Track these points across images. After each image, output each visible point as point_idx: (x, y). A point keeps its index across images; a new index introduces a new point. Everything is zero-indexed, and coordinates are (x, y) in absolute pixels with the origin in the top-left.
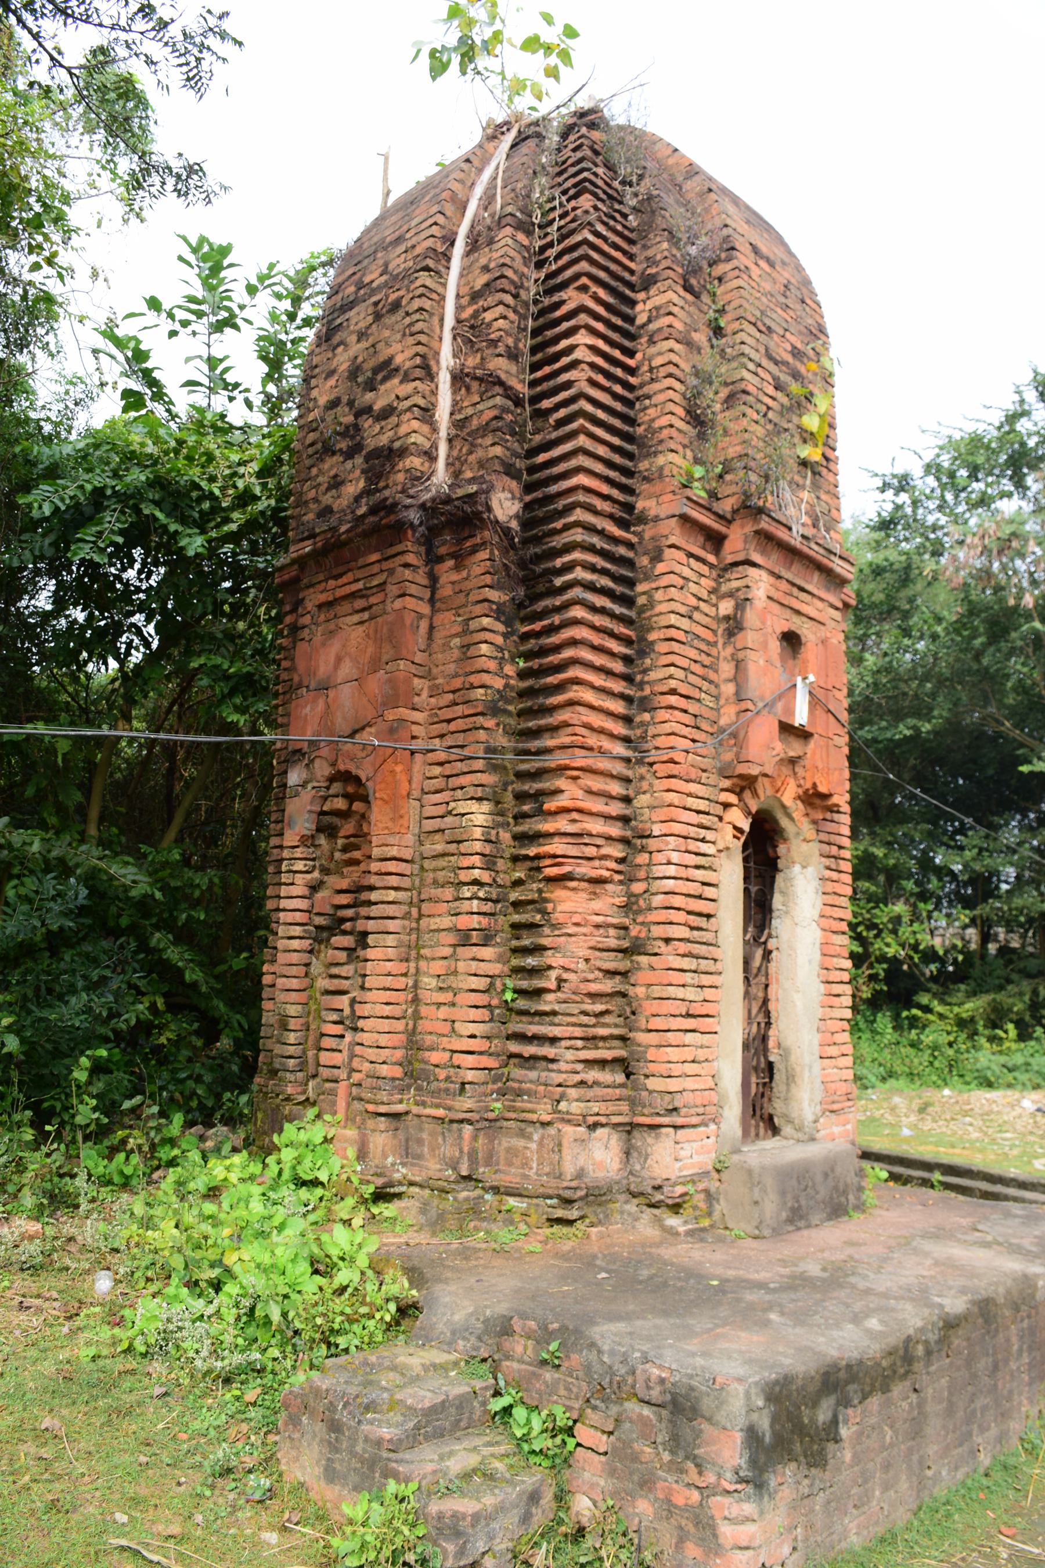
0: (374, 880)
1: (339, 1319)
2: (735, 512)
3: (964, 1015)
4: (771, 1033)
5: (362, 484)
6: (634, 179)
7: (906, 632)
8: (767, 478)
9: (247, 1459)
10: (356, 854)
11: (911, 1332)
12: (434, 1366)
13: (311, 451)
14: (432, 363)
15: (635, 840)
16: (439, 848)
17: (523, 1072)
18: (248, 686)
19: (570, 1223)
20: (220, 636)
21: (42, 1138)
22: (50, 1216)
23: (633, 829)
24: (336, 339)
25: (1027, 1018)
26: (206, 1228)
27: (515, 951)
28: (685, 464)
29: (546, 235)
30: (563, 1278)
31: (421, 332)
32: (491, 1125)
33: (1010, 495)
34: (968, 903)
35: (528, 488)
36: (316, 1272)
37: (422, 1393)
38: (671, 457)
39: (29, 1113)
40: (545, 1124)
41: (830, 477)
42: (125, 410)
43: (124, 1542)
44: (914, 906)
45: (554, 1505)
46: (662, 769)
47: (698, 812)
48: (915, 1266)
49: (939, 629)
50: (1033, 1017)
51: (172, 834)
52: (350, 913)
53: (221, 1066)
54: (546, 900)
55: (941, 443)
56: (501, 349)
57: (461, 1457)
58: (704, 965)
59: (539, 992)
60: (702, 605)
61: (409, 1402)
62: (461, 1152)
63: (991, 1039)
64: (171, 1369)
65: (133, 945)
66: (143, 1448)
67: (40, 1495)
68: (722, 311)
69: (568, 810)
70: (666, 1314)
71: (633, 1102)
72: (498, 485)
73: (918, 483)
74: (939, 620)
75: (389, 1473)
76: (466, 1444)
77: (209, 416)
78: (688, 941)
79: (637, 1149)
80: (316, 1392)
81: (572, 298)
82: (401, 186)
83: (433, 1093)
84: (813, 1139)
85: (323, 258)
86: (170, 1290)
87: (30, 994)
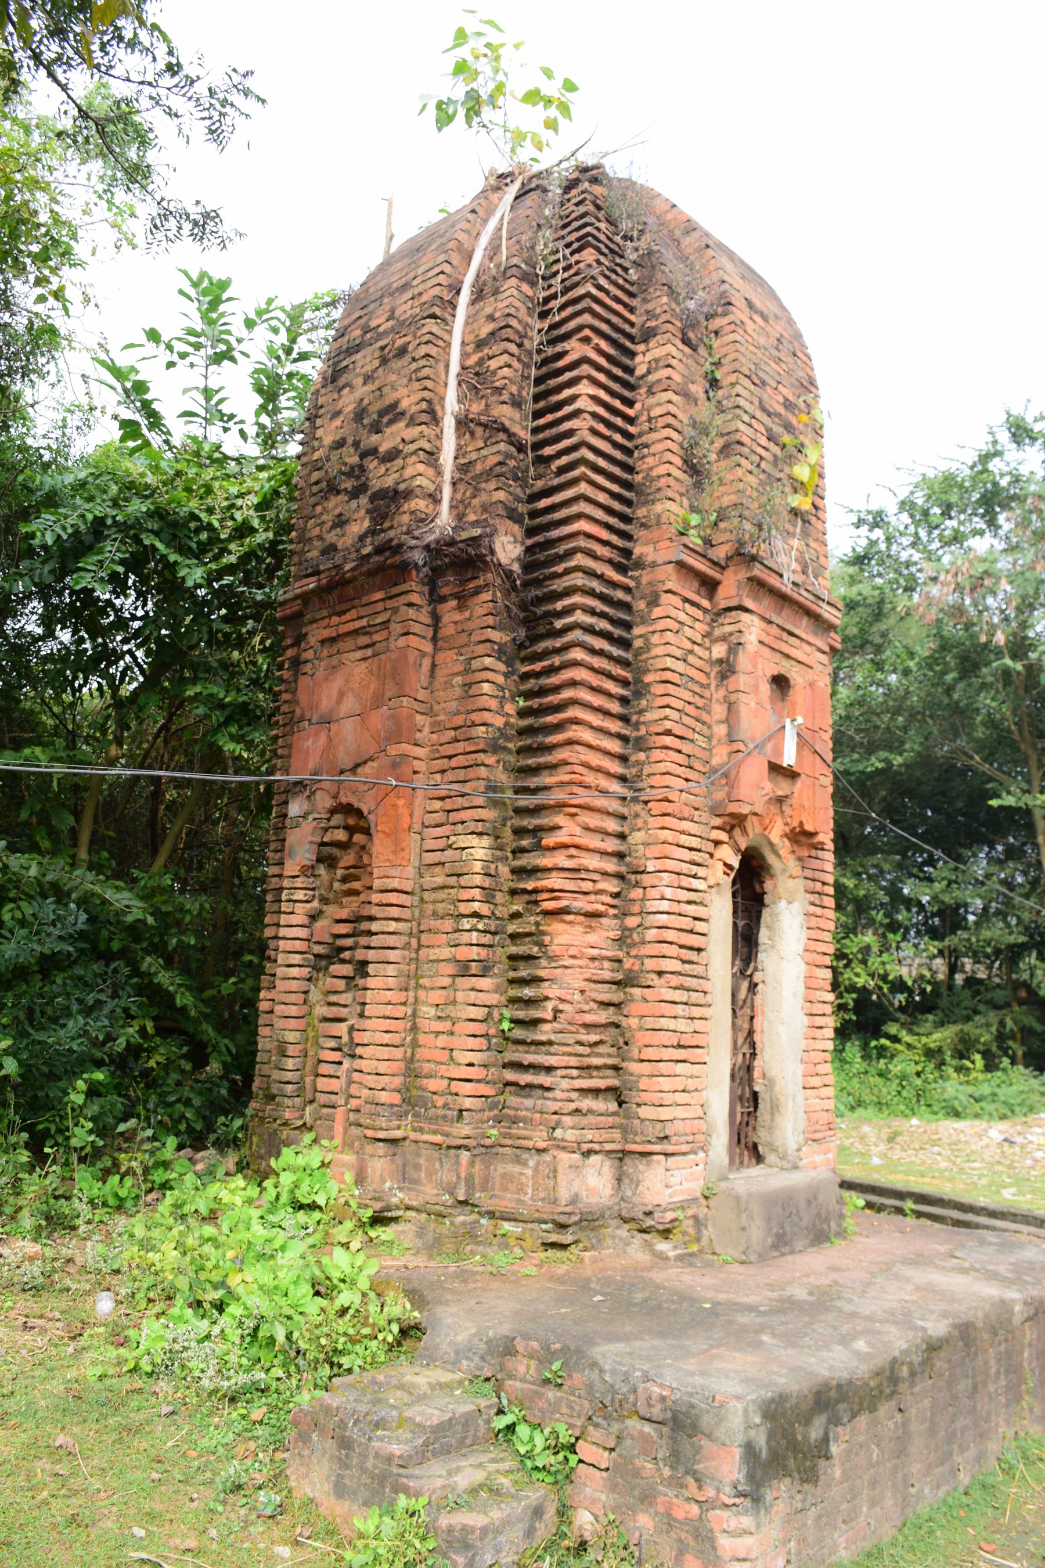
0: (374, 911)
1: (342, 1340)
2: (728, 558)
3: (932, 1046)
4: (756, 1063)
5: (366, 524)
6: (635, 234)
7: (879, 666)
8: (760, 527)
9: (257, 1476)
10: (356, 885)
11: (897, 1353)
12: (440, 1385)
13: (315, 489)
14: (438, 408)
15: (629, 875)
16: (440, 880)
17: (519, 1100)
18: (244, 715)
19: (564, 1247)
20: (215, 664)
21: (39, 1159)
22: (48, 1237)
23: (627, 865)
24: (342, 381)
25: (994, 1049)
26: (208, 1249)
27: (512, 982)
28: (681, 512)
29: (550, 286)
30: (560, 1300)
31: (428, 378)
32: (488, 1151)
33: (981, 533)
34: (935, 934)
35: (530, 532)
36: (317, 1293)
37: (430, 1411)
38: (669, 505)
39: (25, 1135)
40: (540, 1151)
41: (819, 525)
42: (123, 439)
43: (144, 1555)
44: (884, 935)
45: (556, 1519)
46: (656, 807)
47: (691, 849)
48: (902, 1290)
49: (911, 664)
50: (999, 1047)
51: (161, 859)
52: (349, 942)
53: (210, 1090)
54: (543, 933)
55: (915, 480)
56: (505, 397)
57: (468, 1473)
58: (695, 997)
59: (535, 1022)
60: (696, 648)
61: (418, 1419)
62: (458, 1177)
63: (959, 1069)
64: (177, 1389)
65: (126, 971)
66: (154, 1465)
67: (59, 1511)
68: (718, 364)
69: (566, 846)
70: (662, 1335)
71: (625, 1130)
72: (501, 529)
73: (893, 520)
74: (912, 655)
75: (397, 1489)
76: (472, 1460)
77: (207, 447)
78: (680, 974)
79: (628, 1176)
80: (327, 1410)
81: (575, 349)
82: (406, 231)
83: (430, 1120)
84: (796, 1167)
85: (328, 299)
86: (175, 1311)
87: (22, 1015)
